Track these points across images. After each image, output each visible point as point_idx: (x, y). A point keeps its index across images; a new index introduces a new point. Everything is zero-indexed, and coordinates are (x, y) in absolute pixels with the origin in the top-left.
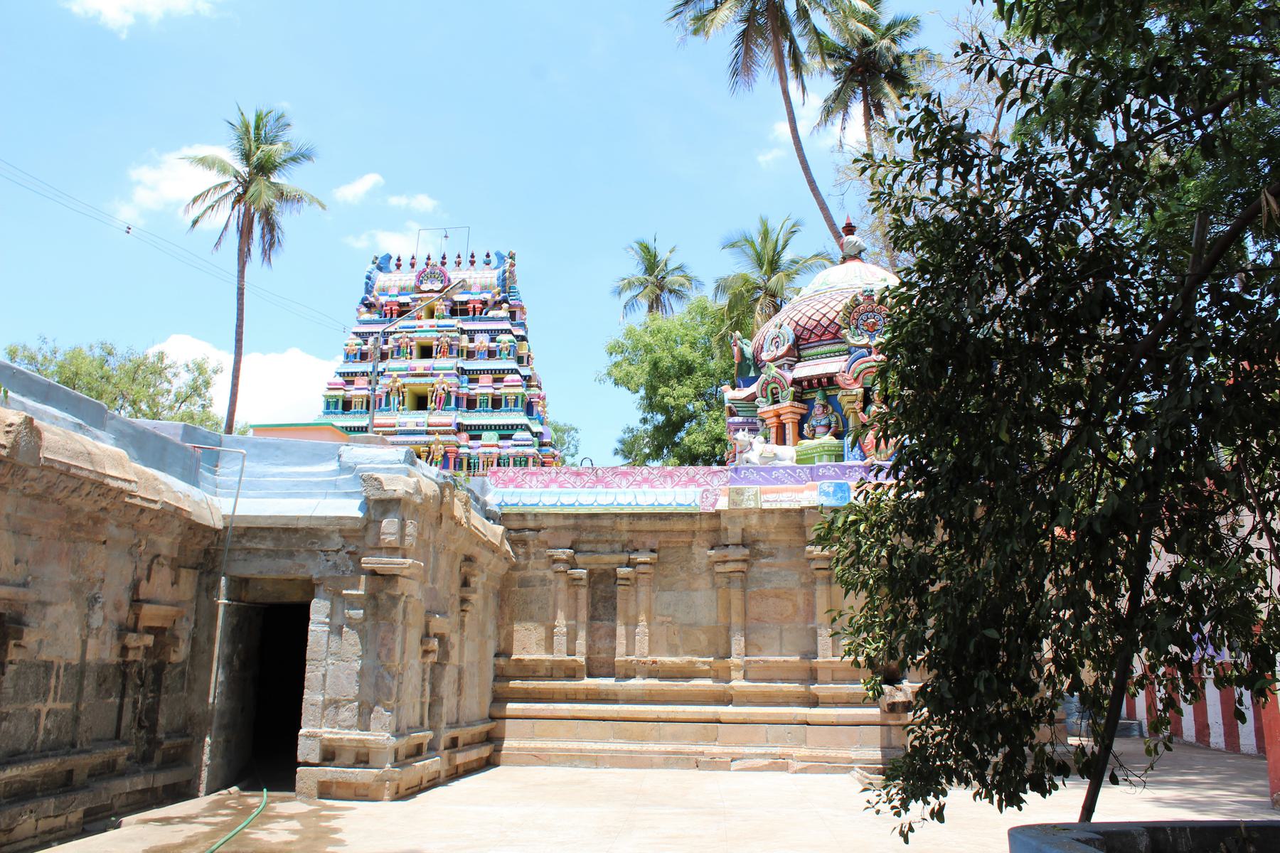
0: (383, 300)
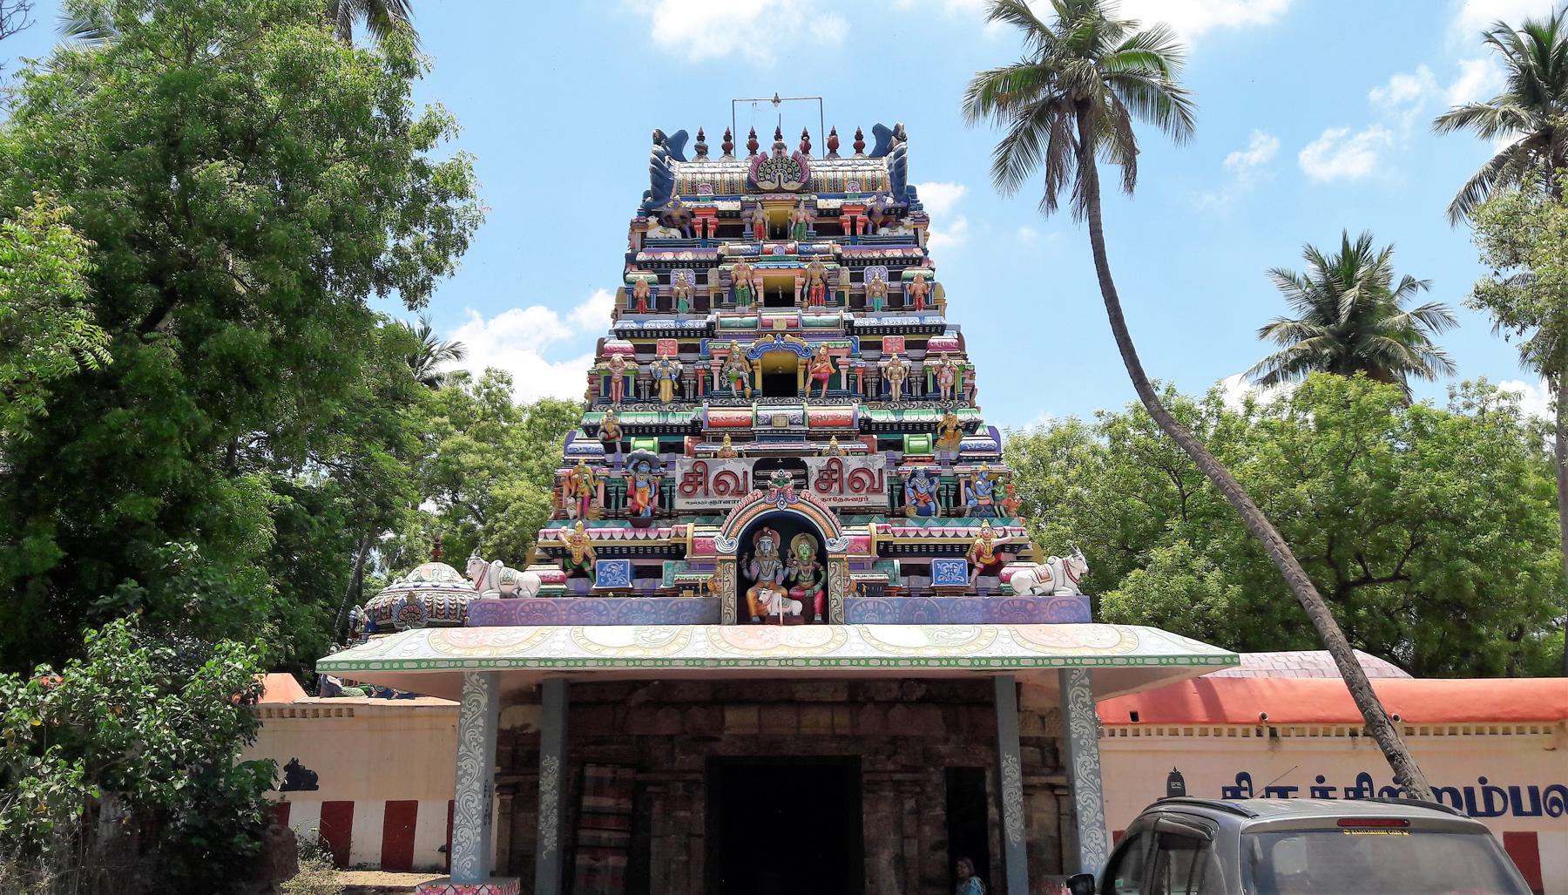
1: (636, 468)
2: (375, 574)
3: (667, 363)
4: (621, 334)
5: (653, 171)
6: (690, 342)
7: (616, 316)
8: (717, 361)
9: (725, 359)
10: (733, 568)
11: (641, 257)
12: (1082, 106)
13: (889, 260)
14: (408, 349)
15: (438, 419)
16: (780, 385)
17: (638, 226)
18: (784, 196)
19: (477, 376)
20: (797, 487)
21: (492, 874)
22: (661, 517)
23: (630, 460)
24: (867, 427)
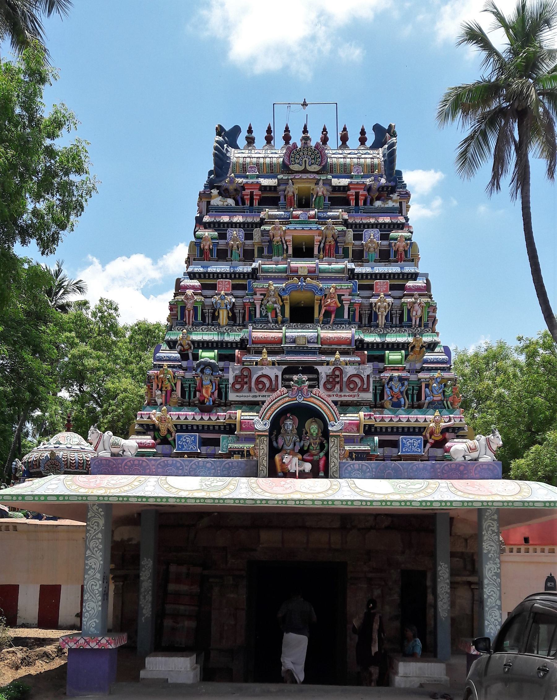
1: (202, 371)
2: (30, 438)
3: (224, 297)
4: (192, 276)
5: (215, 155)
6: (241, 282)
7: (188, 262)
8: (258, 296)
9: (264, 295)
10: (266, 440)
11: (206, 219)
12: (523, 114)
13: (381, 224)
14: (45, 284)
15: (68, 334)
16: (302, 314)
17: (204, 196)
18: (308, 176)
19: (93, 304)
20: (310, 386)
21: (109, 631)
22: (219, 405)
23: (199, 365)
24: (361, 345)
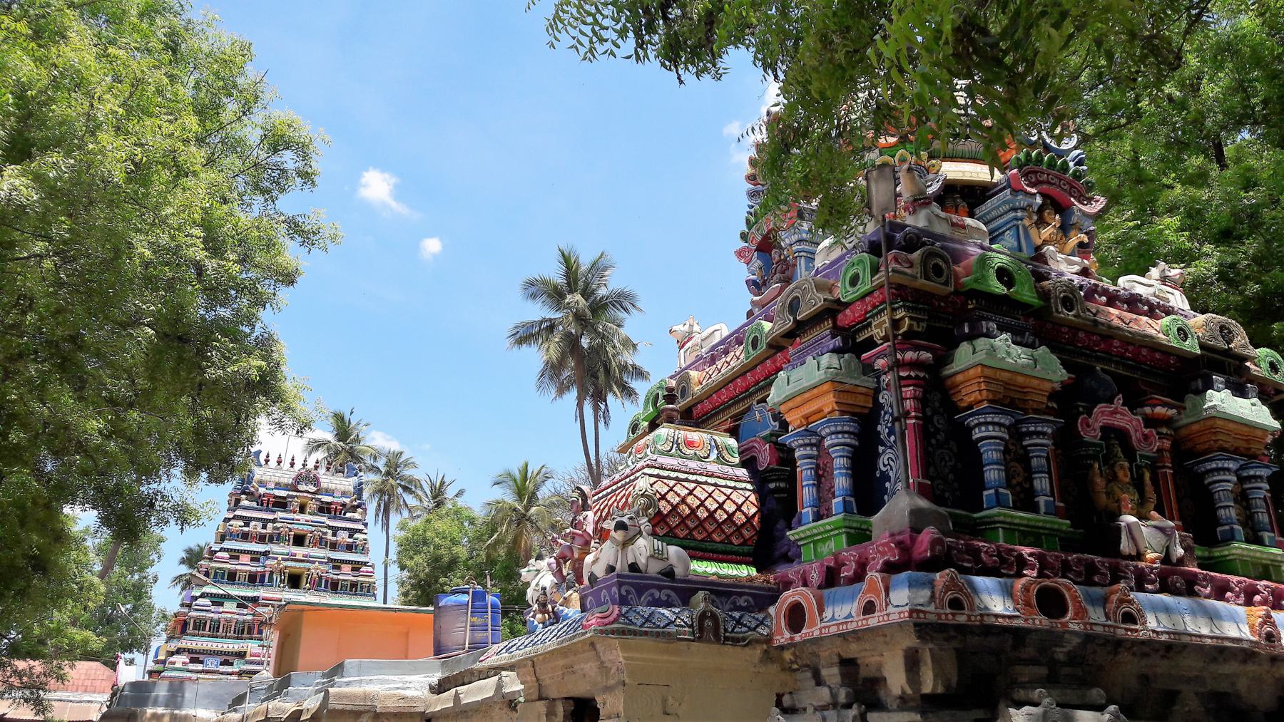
0: (262, 490)
16: (294, 581)
